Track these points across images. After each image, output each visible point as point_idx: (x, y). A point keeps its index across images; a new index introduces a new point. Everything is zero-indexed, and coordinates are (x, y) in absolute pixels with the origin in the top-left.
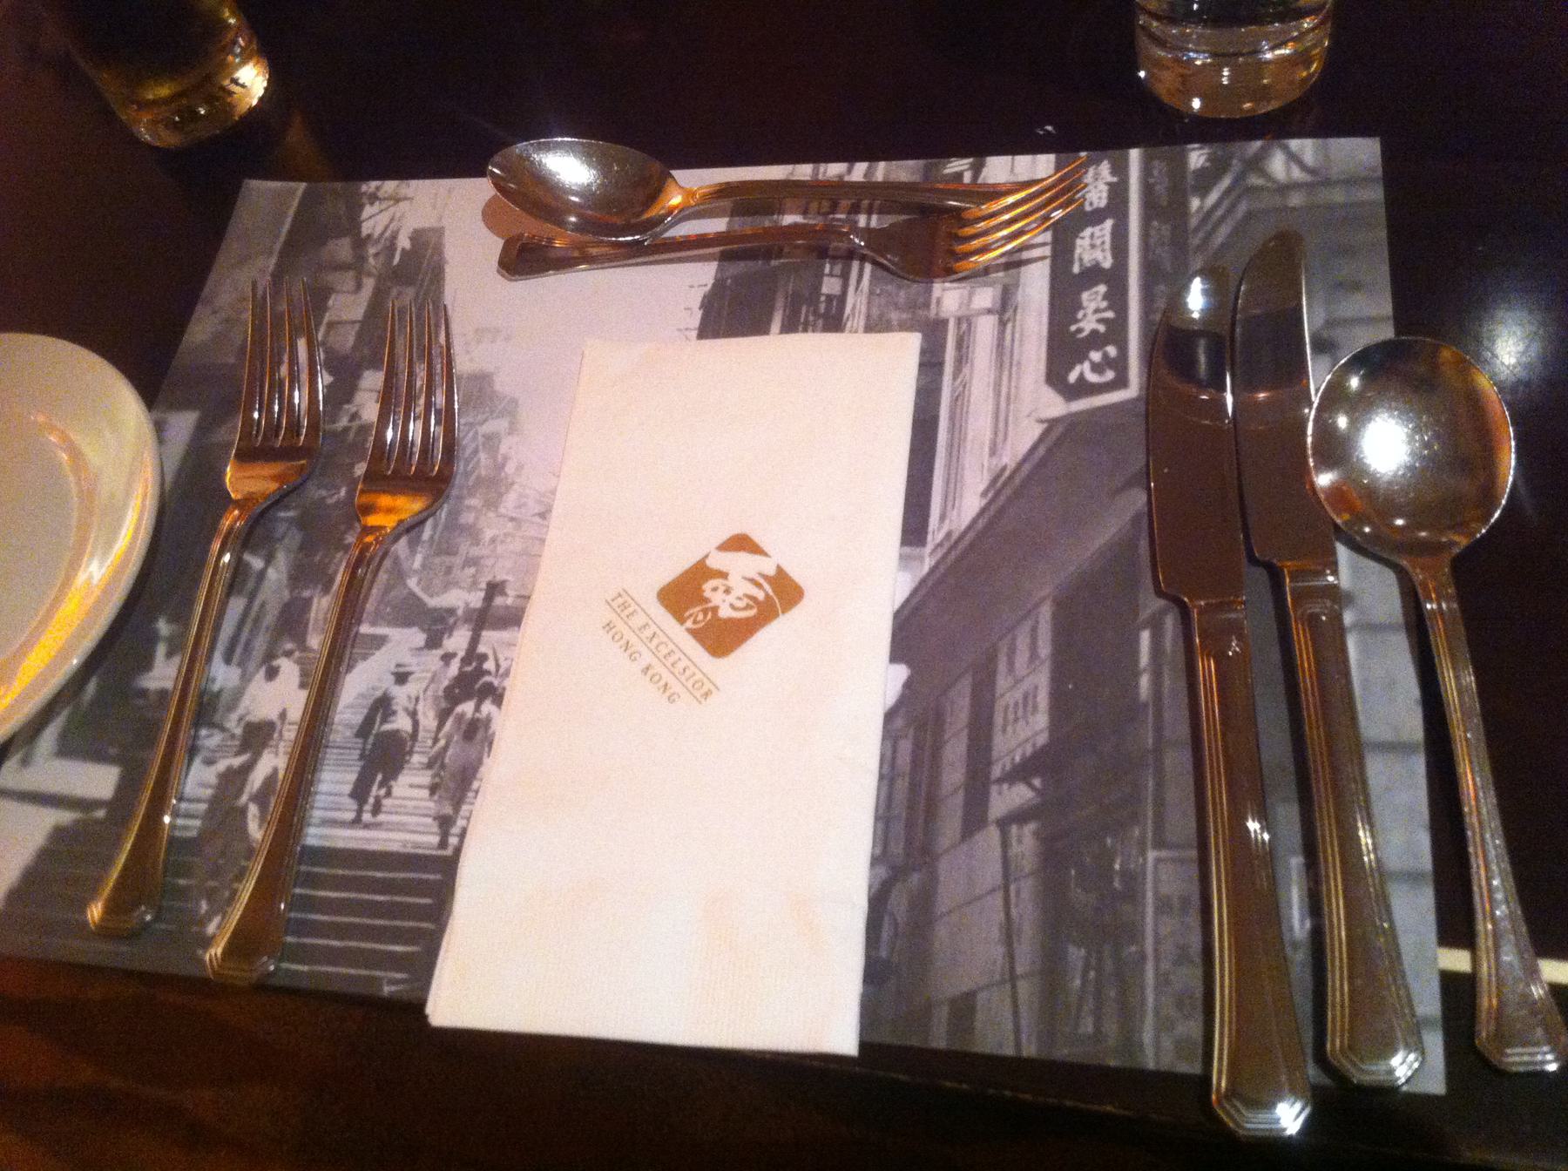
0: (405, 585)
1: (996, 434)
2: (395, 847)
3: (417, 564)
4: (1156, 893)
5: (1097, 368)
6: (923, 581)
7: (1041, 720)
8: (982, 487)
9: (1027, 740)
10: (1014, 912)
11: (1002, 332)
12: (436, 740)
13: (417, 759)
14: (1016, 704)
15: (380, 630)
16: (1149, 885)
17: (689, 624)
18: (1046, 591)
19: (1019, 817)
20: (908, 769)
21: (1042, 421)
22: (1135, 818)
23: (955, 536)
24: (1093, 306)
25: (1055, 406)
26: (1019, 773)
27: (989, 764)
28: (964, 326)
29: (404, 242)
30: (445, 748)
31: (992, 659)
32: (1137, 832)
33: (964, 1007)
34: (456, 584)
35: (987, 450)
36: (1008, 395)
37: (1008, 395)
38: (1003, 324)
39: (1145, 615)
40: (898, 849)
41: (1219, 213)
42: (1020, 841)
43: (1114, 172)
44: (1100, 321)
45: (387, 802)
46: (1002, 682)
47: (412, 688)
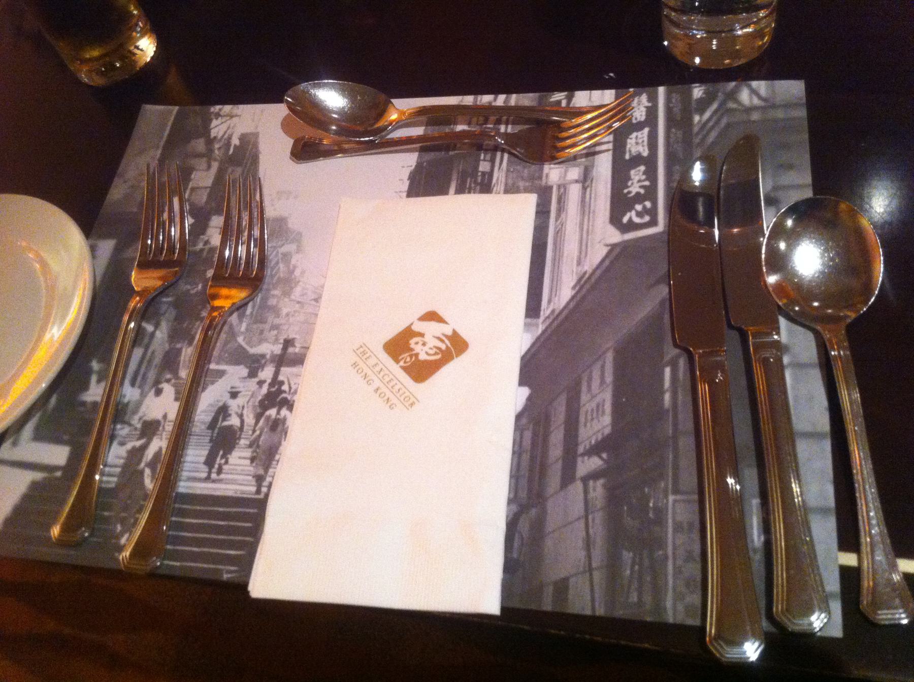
0: (236, 341)
1: (580, 253)
2: (230, 493)
3: (243, 328)
4: (674, 520)
5: (639, 214)
6: (538, 339)
7: (607, 419)
8: (572, 284)
9: (599, 431)
10: (591, 531)
11: (584, 194)
12: (254, 431)
13: (243, 442)
15: (222, 367)
16: (670, 516)
17: (402, 363)
18: (610, 344)
19: (594, 476)
20: (529, 448)
21: (607, 245)
22: (662, 476)
23: (557, 312)
26: (594, 450)
27: (577, 445)
30: (260, 436)
31: (578, 384)
32: (663, 485)
33: (562, 587)
34: (266, 340)
35: (575, 262)
36: (588, 230)
37: (588, 230)
38: (584, 189)
39: (667, 358)
40: (523, 494)
41: (711, 124)
42: (594, 490)
43: (649, 100)
44: (641, 187)
45: (225, 467)
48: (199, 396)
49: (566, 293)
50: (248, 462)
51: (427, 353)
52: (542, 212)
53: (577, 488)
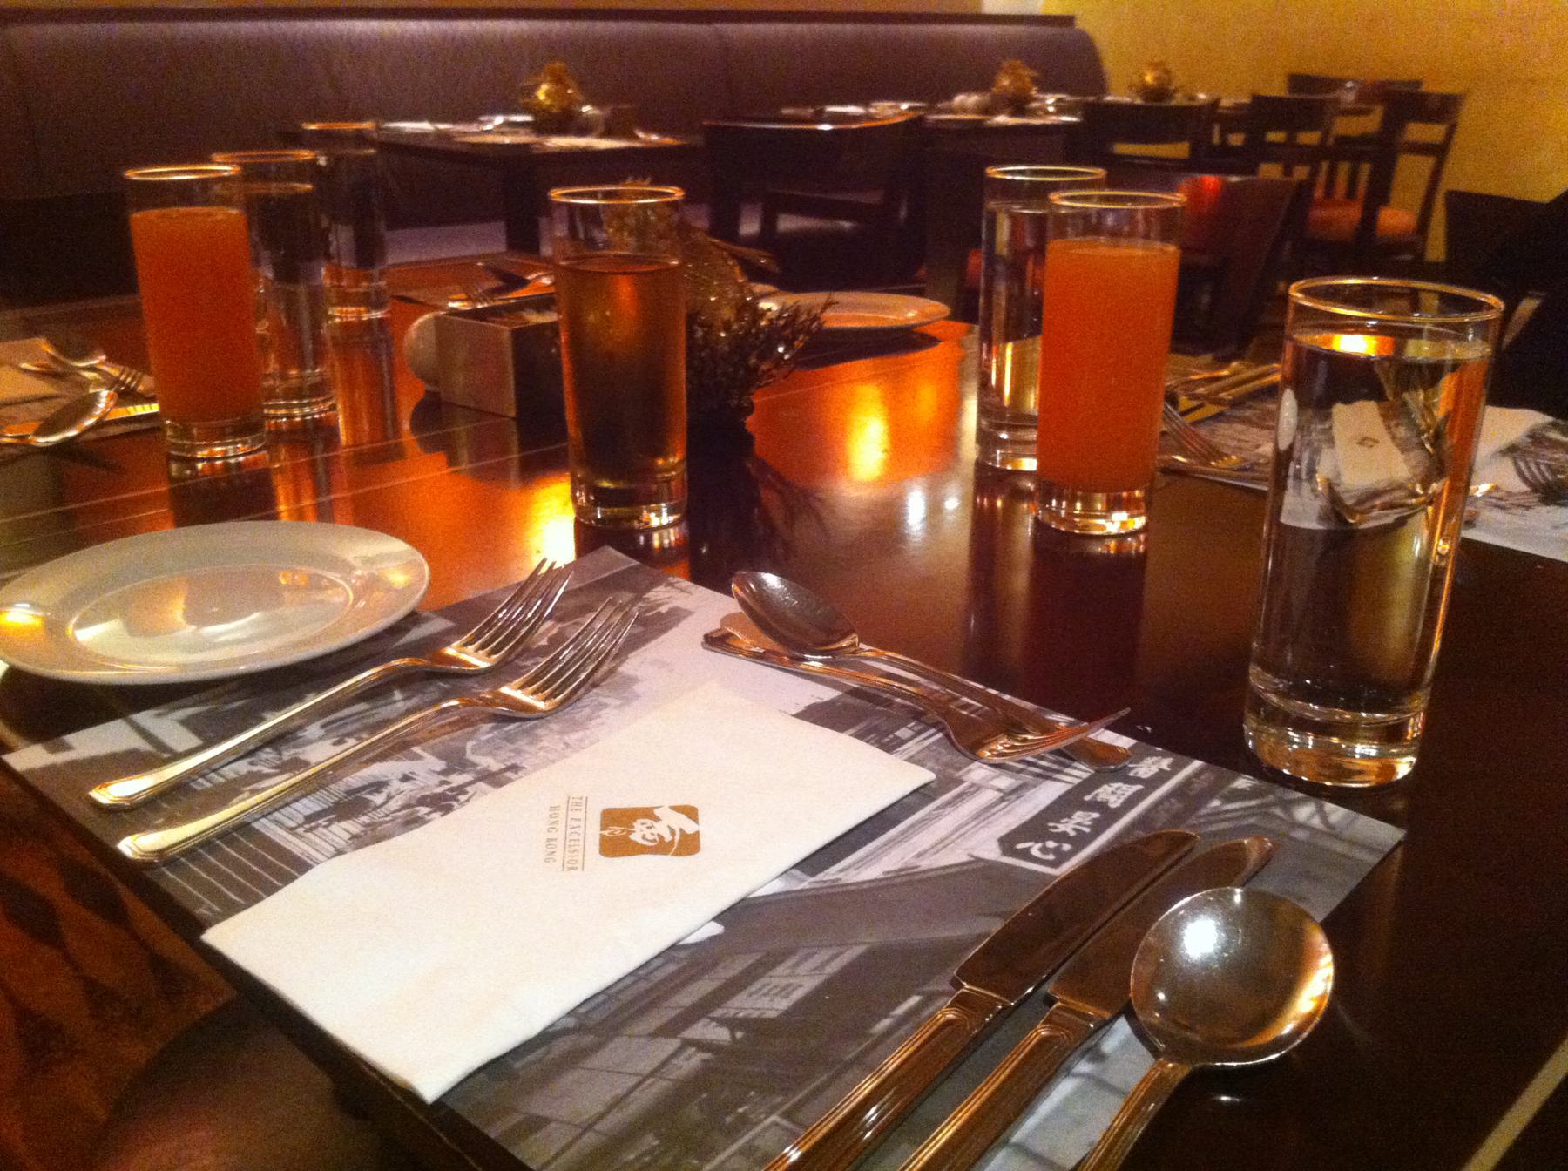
0: (465, 743)
1: (932, 847)
2: (296, 851)
3: (484, 738)
4: (753, 1139)
5: (1044, 850)
6: (788, 892)
7: (783, 1004)
8: (887, 869)
9: (759, 1009)
10: (636, 1093)
11: (996, 804)
12: (387, 815)
13: (365, 819)
14: (776, 987)
15: (424, 754)
16: (752, 1133)
17: (606, 833)
18: (872, 940)
19: (701, 1045)
20: (656, 980)
21: (972, 856)
22: (786, 1092)
23: (840, 883)
24: (1079, 820)
26: (732, 1023)
27: (719, 1006)
29: (664, 609)
30: (387, 822)
31: (793, 952)
32: (779, 1099)
33: (536, 1124)
34: (494, 756)
35: (916, 853)
36: (964, 834)
37: (964, 834)
38: (1002, 800)
40: (597, 1017)
41: (1229, 815)
42: (688, 1059)
43: (1171, 766)
44: (1074, 829)
45: (320, 829)
46: (780, 970)
47: (406, 786)
49: (872, 872)
51: (644, 837)
52: (923, 795)
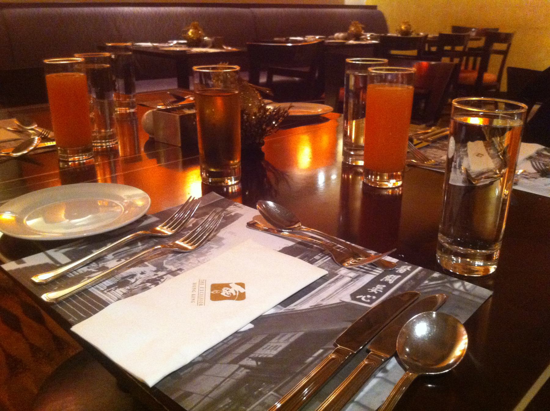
0: (163, 261)
1: (327, 297)
2: (104, 299)
3: (170, 259)
4: (264, 400)
5: (366, 298)
6: (276, 313)
7: (275, 352)
8: (311, 305)
9: (266, 354)
10: (223, 384)
11: (349, 282)
12: (136, 286)
13: (128, 287)
15: (149, 265)
16: (264, 398)
17: (212, 292)
18: (306, 330)
19: (246, 367)
20: (230, 344)
21: (341, 300)
22: (276, 383)
23: (295, 310)
25: (348, 299)
26: (257, 359)
27: (252, 353)
28: (341, 277)
30: (136, 289)
31: (278, 334)
32: (273, 386)
33: (188, 394)
35: (321, 299)
36: (338, 293)
37: (338, 293)
38: (351, 281)
39: (327, 346)
40: (209, 357)
41: (431, 286)
42: (241, 372)
43: (411, 269)
44: (377, 291)
45: (112, 291)
48: (372, 379)
49: (306, 306)
50: (122, 293)
52: (324, 279)
53: (236, 366)
